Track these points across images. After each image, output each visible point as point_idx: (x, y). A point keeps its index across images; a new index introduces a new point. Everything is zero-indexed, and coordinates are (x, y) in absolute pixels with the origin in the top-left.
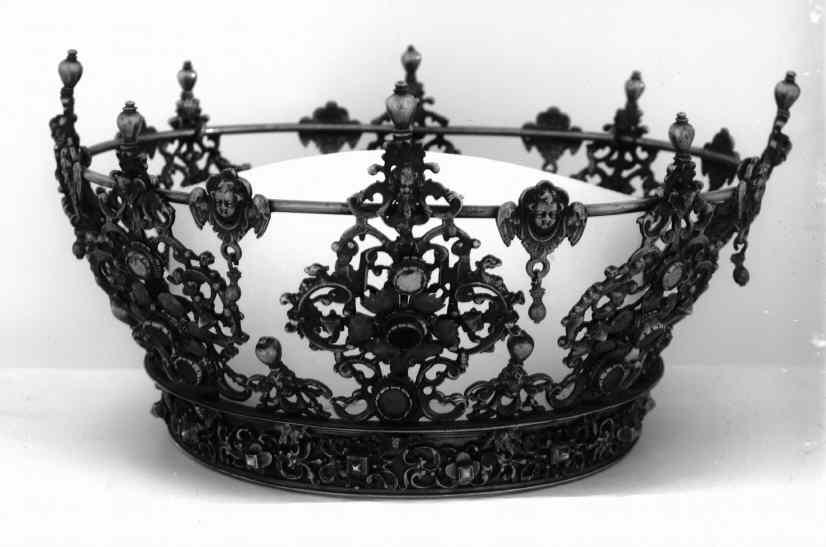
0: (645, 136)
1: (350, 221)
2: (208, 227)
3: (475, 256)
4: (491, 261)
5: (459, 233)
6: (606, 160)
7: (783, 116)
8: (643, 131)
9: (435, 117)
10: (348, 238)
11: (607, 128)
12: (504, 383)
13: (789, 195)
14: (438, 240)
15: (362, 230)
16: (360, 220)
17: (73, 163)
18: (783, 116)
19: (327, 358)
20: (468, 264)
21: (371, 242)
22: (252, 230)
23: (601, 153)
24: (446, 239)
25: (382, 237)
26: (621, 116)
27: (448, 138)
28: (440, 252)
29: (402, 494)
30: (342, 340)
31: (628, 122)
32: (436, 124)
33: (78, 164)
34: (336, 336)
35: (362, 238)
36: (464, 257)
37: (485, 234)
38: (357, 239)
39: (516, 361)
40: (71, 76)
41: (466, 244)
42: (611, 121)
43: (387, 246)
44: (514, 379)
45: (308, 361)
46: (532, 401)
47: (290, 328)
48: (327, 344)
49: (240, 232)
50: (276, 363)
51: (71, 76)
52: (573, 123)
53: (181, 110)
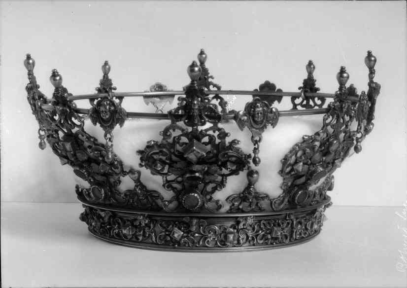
0: (318, 92)
1: (168, 122)
2: (98, 125)
3: (228, 140)
4: (234, 142)
5: (219, 130)
6: (301, 104)
7: (372, 72)
8: (318, 89)
9: (215, 86)
10: (167, 130)
11: (300, 88)
12: (245, 195)
13: (389, 110)
14: (211, 132)
15: (173, 127)
16: (173, 122)
17: (314, 153)
18: (372, 72)
19: (159, 179)
20: (225, 143)
21: (178, 133)
22: (118, 125)
23: (298, 101)
24: (214, 132)
25: (183, 130)
26: (306, 82)
27: (220, 95)
28: (211, 138)
29: (293, 244)
30: (165, 171)
31: (309, 86)
32: (215, 89)
33: (318, 154)
34: (163, 169)
35: (174, 130)
36: (223, 140)
37: (232, 129)
38: (171, 131)
39: (250, 184)
40: (29, 62)
41: (223, 135)
42: (302, 85)
43: (186, 134)
44: (250, 193)
45: (154, 181)
46: (259, 205)
47: (141, 165)
48: (159, 173)
49: (112, 127)
50: (138, 181)
51: (29, 62)
52: (278, 87)
53: (102, 83)
